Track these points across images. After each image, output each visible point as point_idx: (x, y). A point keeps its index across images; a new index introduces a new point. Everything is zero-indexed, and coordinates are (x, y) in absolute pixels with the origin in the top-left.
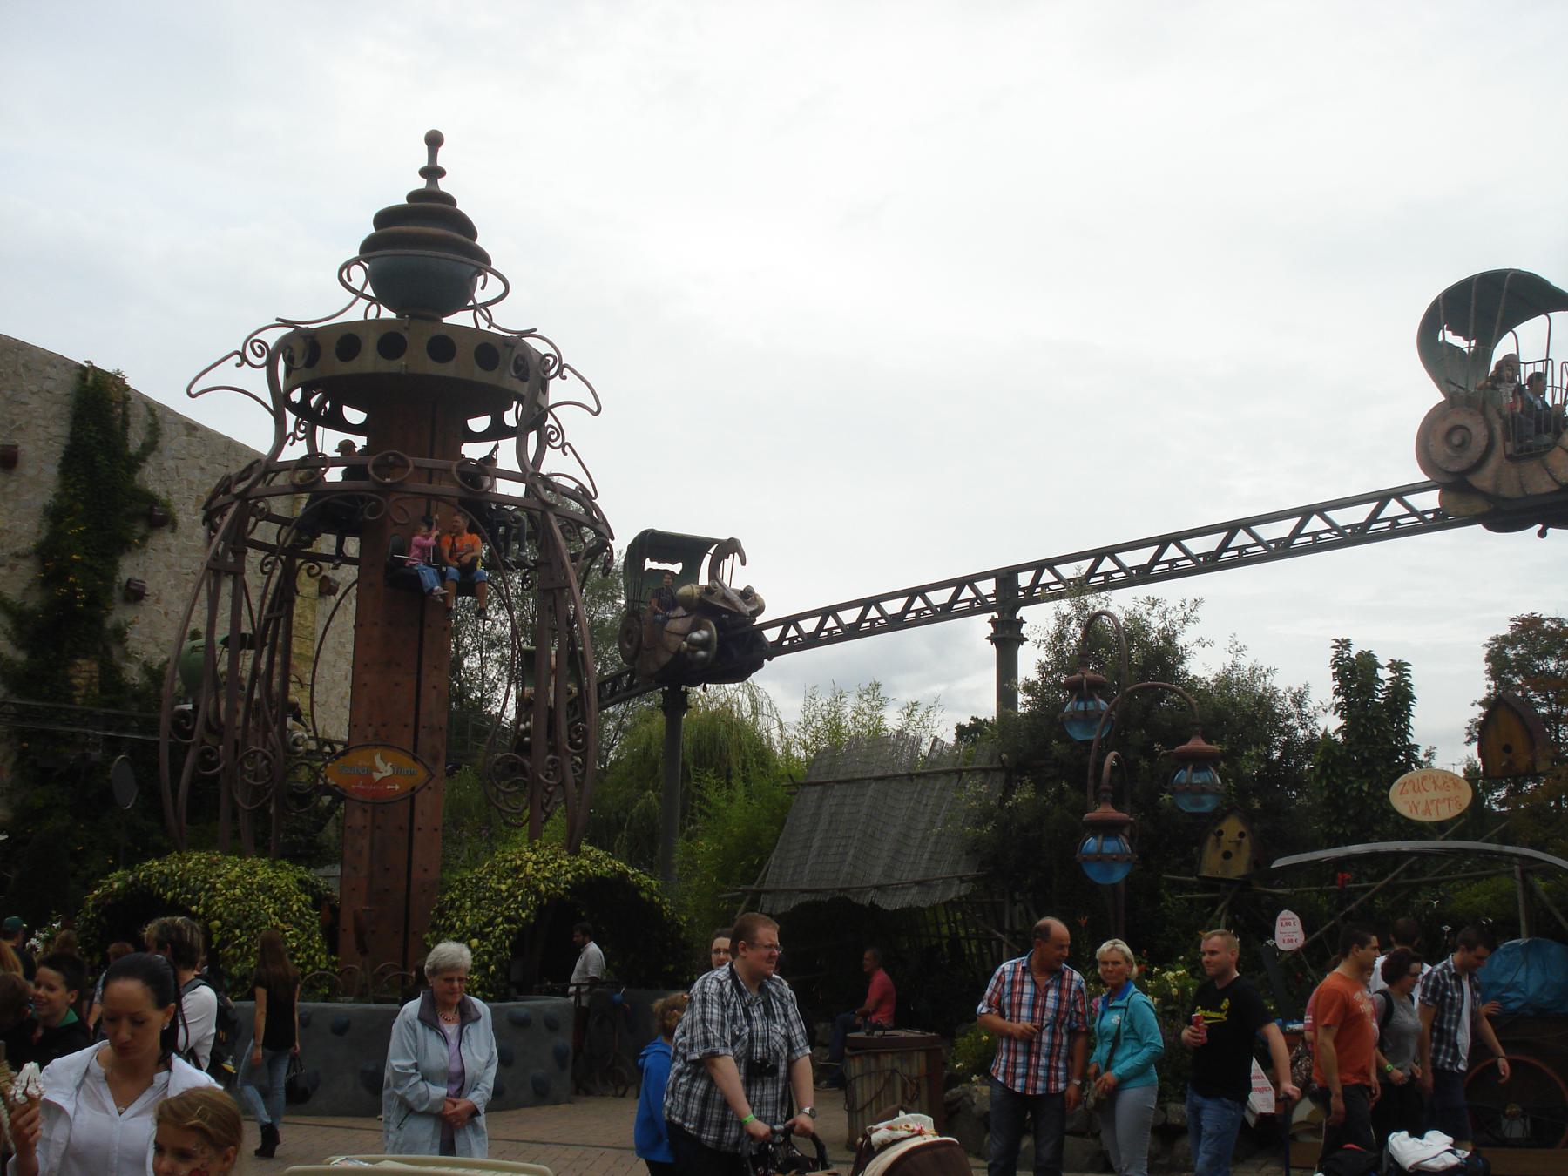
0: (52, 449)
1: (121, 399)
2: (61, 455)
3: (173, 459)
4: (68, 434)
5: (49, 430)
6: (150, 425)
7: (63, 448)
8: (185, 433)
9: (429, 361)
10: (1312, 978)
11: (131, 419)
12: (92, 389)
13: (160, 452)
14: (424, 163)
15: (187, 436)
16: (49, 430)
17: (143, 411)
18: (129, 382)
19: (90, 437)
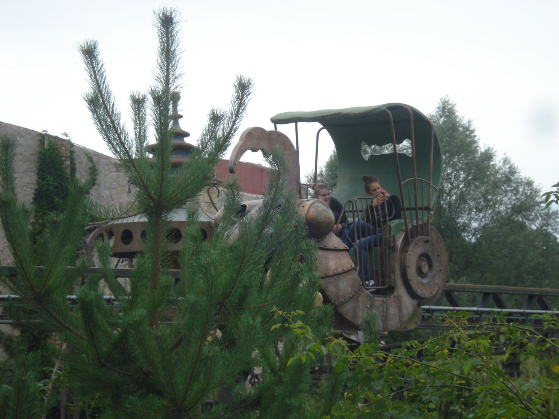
0: (26, 192)
1: (69, 155)
2: (33, 196)
3: (108, 189)
4: (35, 182)
5: (23, 180)
6: (90, 168)
7: (34, 192)
8: (115, 170)
9: (122, 244)
10: (440, 316)
11: (77, 166)
12: (49, 150)
13: (99, 186)
14: (159, 87)
15: (116, 172)
16: (23, 180)
17: (84, 159)
18: (74, 141)
19: (50, 185)
